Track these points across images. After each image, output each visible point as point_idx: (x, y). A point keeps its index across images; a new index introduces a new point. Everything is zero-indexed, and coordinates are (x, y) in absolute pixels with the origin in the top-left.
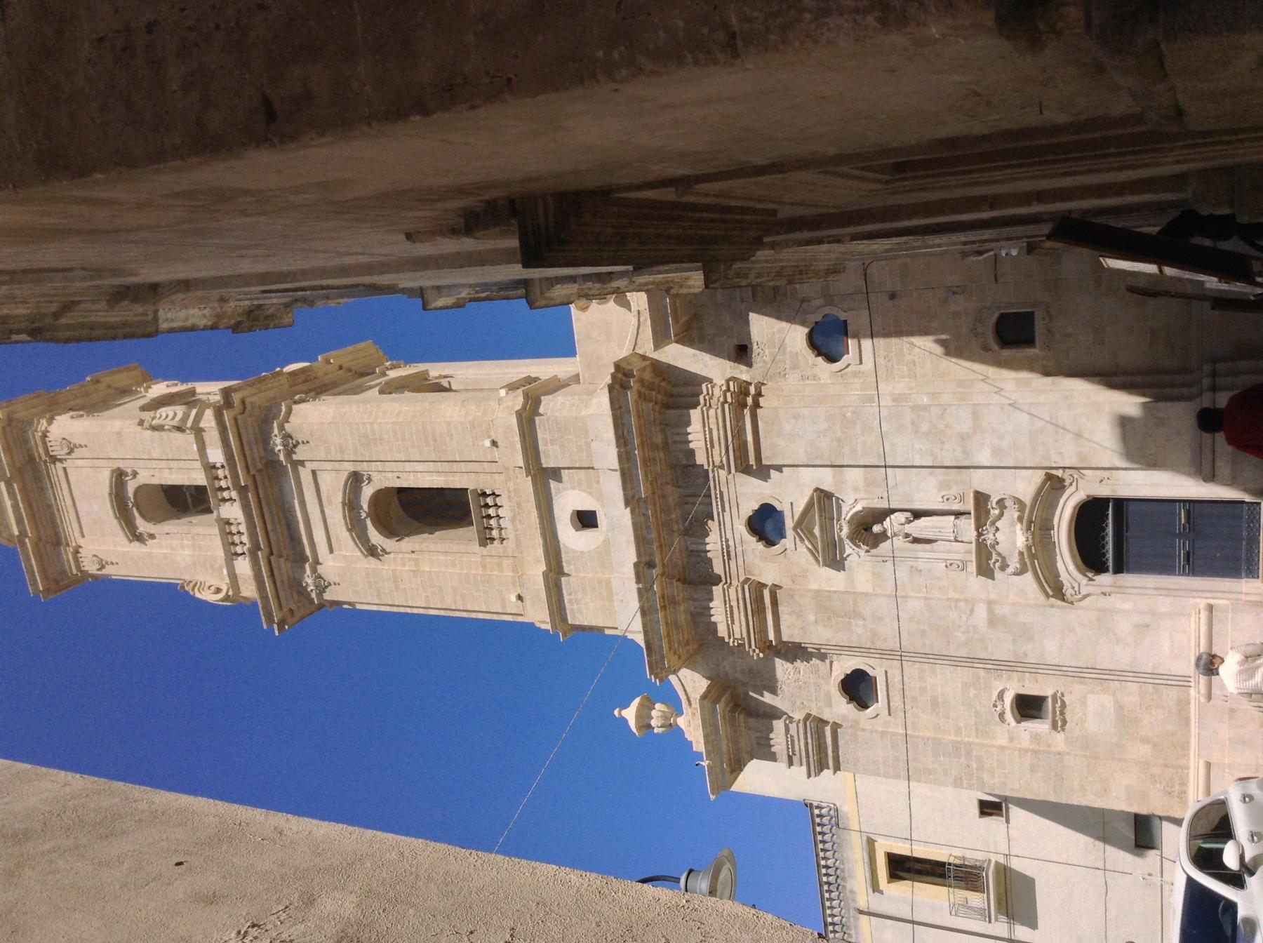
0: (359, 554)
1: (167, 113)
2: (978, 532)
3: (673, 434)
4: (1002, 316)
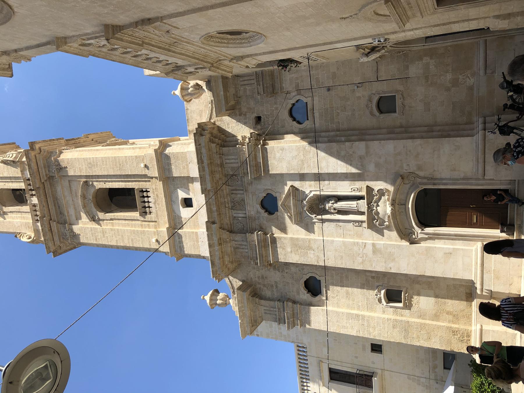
0: (88, 220)
2: (368, 206)
3: (225, 159)
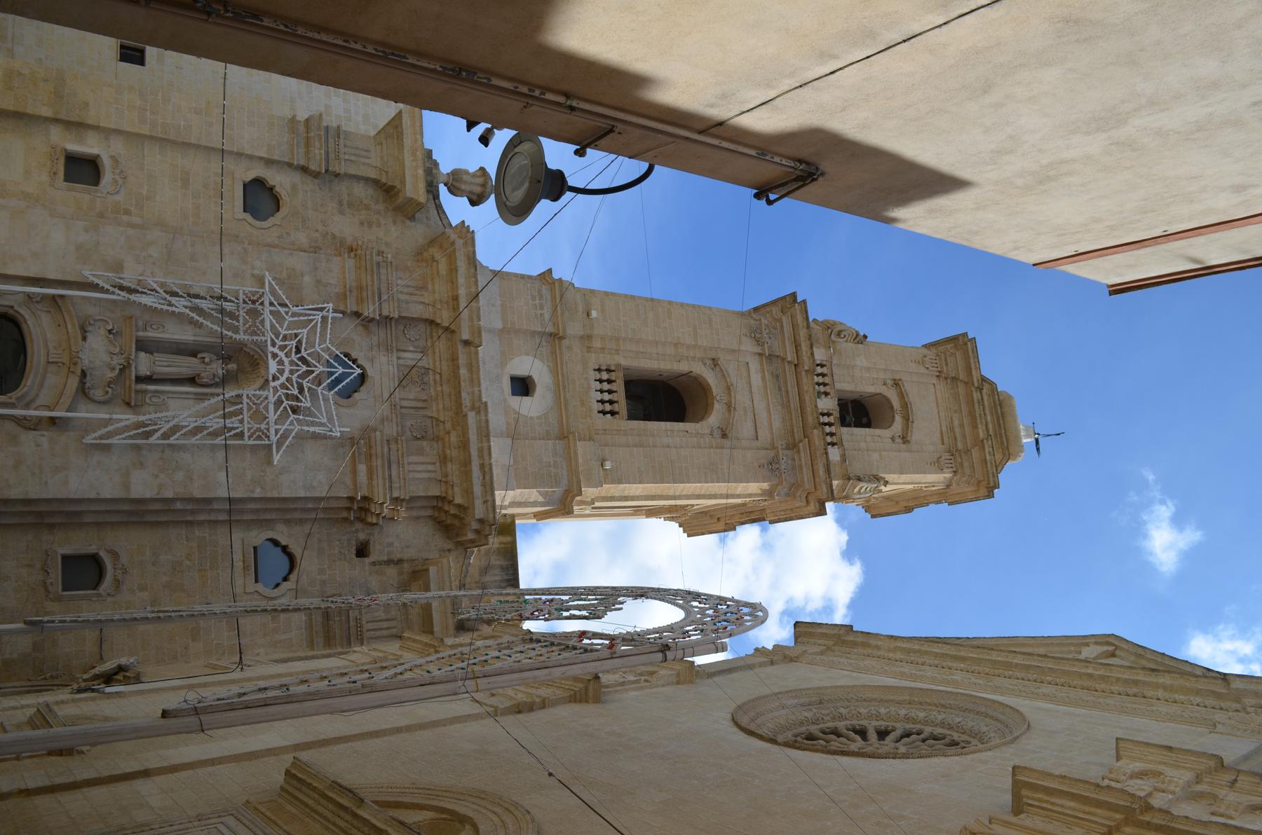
3: (435, 471)
4: (96, 586)
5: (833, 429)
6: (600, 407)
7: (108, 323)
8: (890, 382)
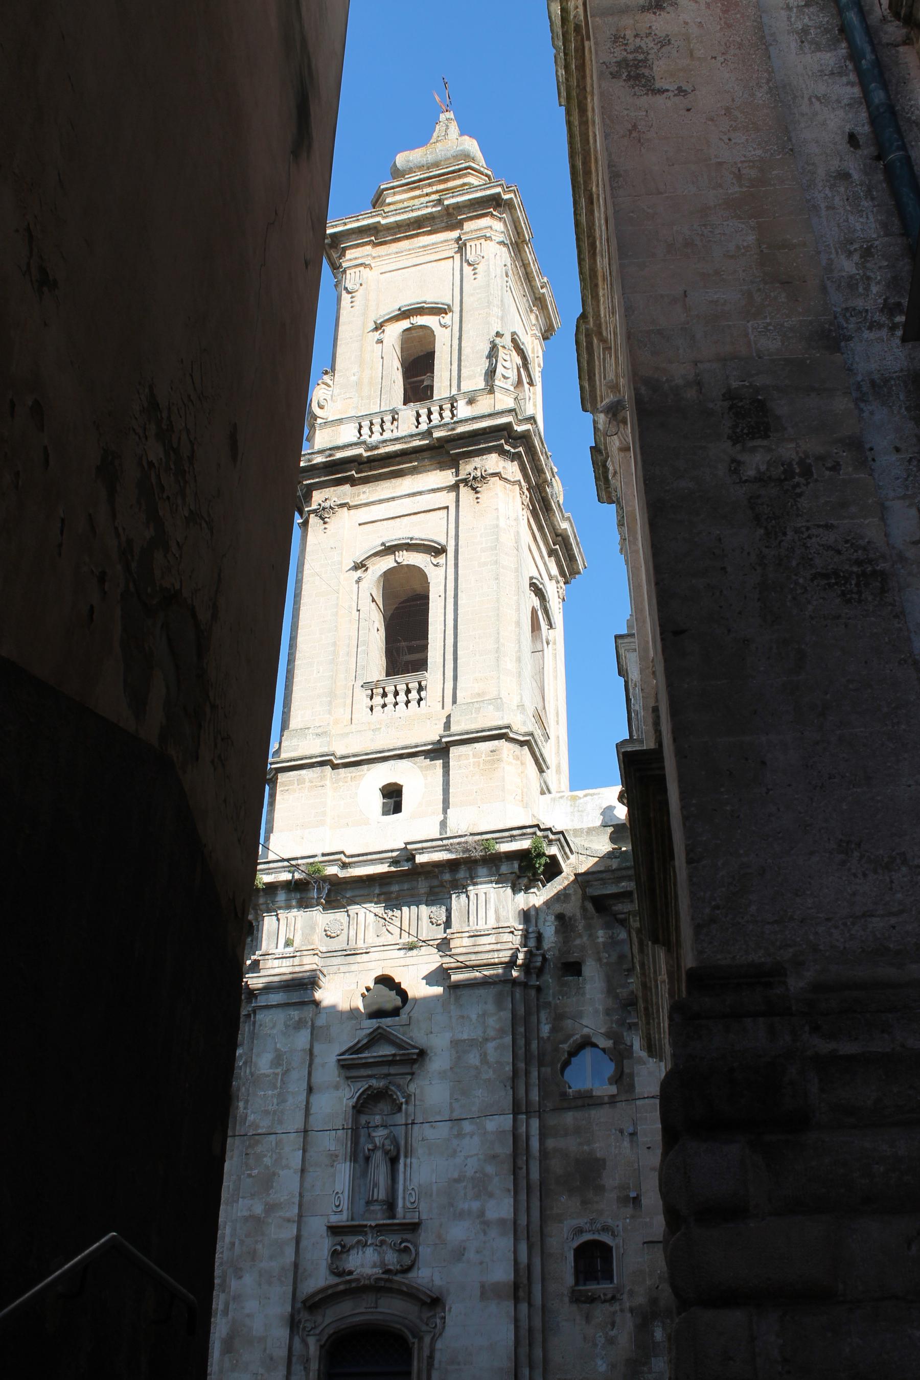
1: (680, 576)
5: (435, 409)
6: (413, 704)
7: (335, 1250)
8: (376, 335)
